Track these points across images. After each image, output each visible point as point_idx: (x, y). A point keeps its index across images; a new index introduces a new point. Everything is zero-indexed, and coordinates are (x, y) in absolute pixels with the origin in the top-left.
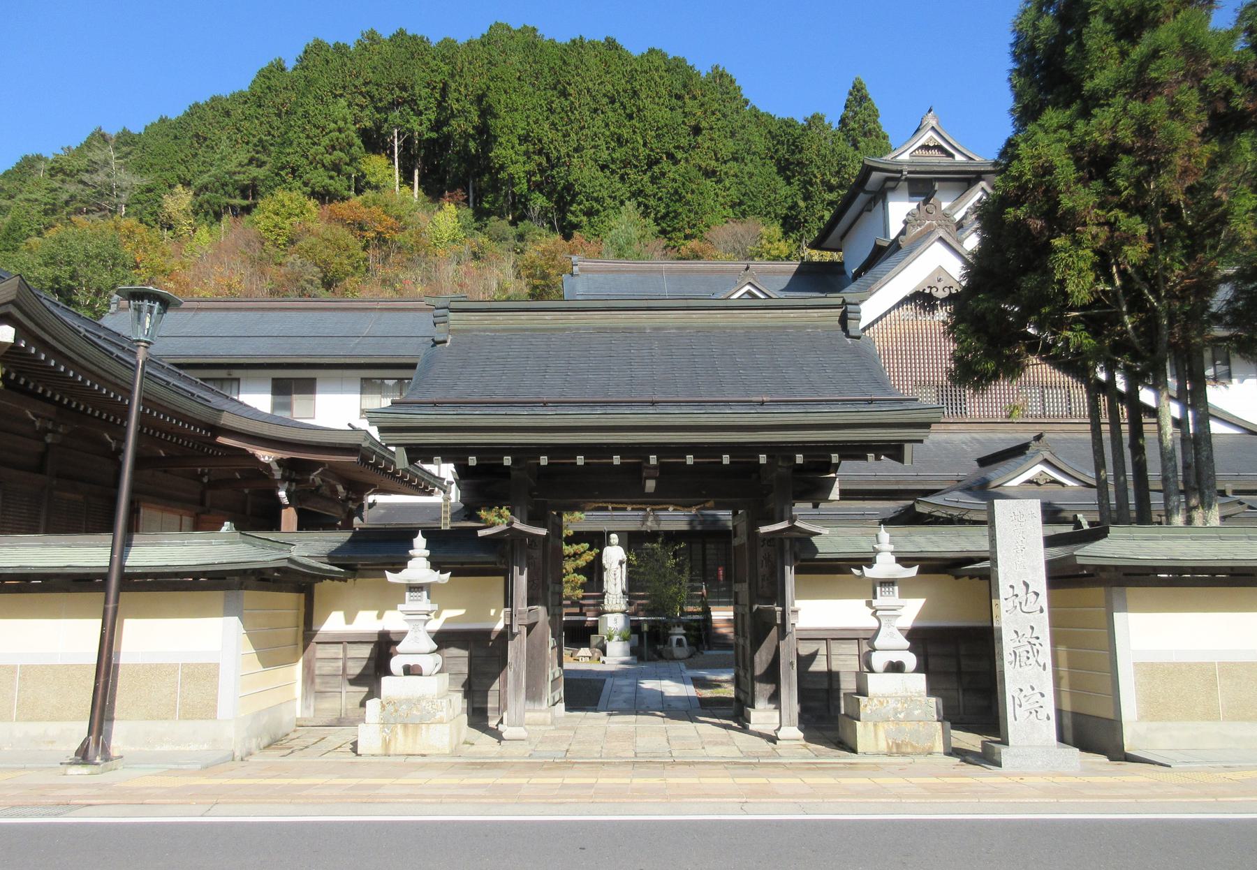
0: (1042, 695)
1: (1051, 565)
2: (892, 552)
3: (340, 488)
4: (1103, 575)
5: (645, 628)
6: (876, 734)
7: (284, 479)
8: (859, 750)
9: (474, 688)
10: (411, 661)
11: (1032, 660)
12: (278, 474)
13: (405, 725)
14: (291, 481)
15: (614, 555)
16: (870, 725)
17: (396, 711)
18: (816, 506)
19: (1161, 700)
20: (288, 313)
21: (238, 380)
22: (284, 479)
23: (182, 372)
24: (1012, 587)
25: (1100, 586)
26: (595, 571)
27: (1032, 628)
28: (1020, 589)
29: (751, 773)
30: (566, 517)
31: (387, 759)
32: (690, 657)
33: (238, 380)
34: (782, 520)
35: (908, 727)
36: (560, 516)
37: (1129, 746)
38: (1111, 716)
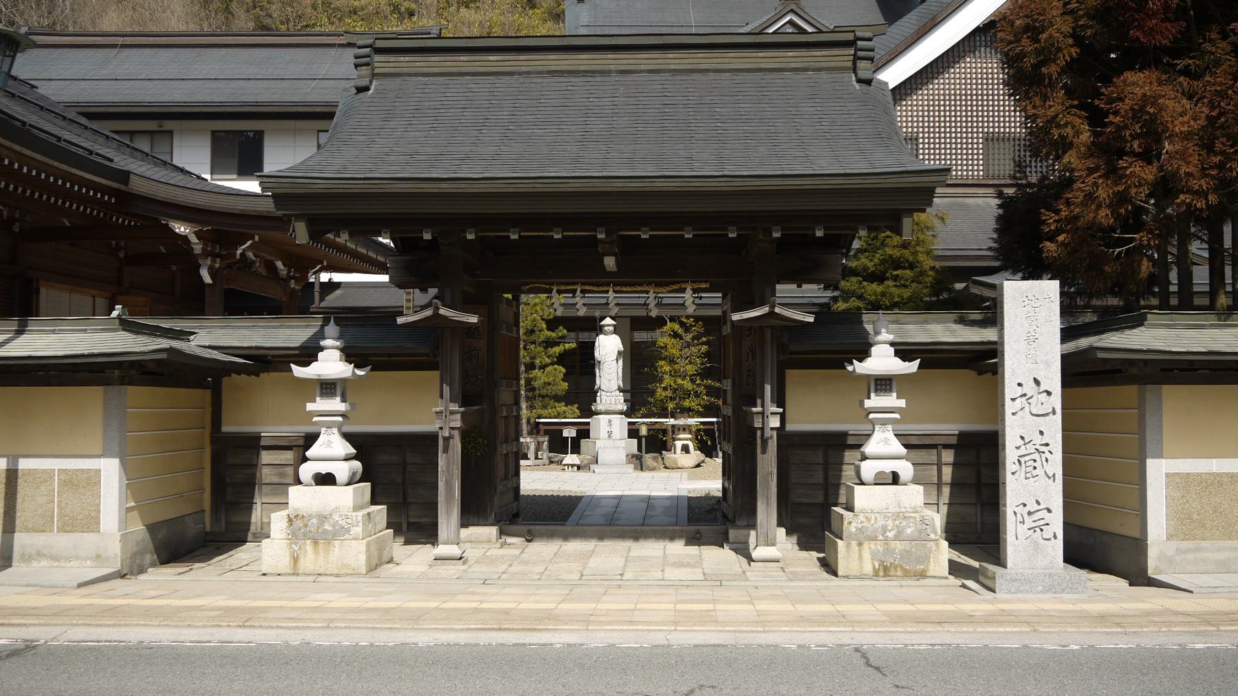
0: (1049, 511)
1: (1068, 361)
2: (892, 344)
3: (279, 264)
4: (1133, 371)
5: (644, 431)
6: (860, 557)
7: (205, 254)
8: (840, 573)
9: (409, 500)
10: (324, 468)
11: (1039, 471)
12: (198, 247)
13: (316, 543)
14: (215, 256)
15: (608, 347)
16: (854, 543)
17: (306, 526)
18: (799, 286)
19: (1195, 517)
20: (230, 50)
21: (171, 132)
22: (205, 254)
23: (94, 125)
24: (1020, 385)
25: (1133, 384)
26: (582, 365)
27: (1041, 433)
28: (1030, 388)
29: (761, 592)
30: (1050, 289)
31: (294, 578)
32: (698, 466)
33: (171, 132)
34: (762, 304)
35: (898, 546)
36: (516, 299)
37: (1153, 567)
38: (1136, 534)
